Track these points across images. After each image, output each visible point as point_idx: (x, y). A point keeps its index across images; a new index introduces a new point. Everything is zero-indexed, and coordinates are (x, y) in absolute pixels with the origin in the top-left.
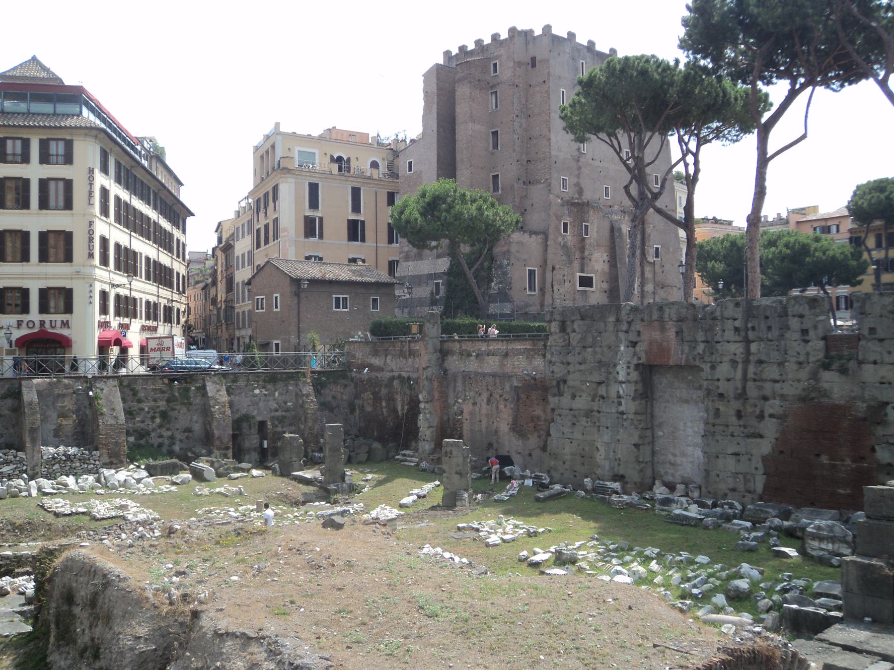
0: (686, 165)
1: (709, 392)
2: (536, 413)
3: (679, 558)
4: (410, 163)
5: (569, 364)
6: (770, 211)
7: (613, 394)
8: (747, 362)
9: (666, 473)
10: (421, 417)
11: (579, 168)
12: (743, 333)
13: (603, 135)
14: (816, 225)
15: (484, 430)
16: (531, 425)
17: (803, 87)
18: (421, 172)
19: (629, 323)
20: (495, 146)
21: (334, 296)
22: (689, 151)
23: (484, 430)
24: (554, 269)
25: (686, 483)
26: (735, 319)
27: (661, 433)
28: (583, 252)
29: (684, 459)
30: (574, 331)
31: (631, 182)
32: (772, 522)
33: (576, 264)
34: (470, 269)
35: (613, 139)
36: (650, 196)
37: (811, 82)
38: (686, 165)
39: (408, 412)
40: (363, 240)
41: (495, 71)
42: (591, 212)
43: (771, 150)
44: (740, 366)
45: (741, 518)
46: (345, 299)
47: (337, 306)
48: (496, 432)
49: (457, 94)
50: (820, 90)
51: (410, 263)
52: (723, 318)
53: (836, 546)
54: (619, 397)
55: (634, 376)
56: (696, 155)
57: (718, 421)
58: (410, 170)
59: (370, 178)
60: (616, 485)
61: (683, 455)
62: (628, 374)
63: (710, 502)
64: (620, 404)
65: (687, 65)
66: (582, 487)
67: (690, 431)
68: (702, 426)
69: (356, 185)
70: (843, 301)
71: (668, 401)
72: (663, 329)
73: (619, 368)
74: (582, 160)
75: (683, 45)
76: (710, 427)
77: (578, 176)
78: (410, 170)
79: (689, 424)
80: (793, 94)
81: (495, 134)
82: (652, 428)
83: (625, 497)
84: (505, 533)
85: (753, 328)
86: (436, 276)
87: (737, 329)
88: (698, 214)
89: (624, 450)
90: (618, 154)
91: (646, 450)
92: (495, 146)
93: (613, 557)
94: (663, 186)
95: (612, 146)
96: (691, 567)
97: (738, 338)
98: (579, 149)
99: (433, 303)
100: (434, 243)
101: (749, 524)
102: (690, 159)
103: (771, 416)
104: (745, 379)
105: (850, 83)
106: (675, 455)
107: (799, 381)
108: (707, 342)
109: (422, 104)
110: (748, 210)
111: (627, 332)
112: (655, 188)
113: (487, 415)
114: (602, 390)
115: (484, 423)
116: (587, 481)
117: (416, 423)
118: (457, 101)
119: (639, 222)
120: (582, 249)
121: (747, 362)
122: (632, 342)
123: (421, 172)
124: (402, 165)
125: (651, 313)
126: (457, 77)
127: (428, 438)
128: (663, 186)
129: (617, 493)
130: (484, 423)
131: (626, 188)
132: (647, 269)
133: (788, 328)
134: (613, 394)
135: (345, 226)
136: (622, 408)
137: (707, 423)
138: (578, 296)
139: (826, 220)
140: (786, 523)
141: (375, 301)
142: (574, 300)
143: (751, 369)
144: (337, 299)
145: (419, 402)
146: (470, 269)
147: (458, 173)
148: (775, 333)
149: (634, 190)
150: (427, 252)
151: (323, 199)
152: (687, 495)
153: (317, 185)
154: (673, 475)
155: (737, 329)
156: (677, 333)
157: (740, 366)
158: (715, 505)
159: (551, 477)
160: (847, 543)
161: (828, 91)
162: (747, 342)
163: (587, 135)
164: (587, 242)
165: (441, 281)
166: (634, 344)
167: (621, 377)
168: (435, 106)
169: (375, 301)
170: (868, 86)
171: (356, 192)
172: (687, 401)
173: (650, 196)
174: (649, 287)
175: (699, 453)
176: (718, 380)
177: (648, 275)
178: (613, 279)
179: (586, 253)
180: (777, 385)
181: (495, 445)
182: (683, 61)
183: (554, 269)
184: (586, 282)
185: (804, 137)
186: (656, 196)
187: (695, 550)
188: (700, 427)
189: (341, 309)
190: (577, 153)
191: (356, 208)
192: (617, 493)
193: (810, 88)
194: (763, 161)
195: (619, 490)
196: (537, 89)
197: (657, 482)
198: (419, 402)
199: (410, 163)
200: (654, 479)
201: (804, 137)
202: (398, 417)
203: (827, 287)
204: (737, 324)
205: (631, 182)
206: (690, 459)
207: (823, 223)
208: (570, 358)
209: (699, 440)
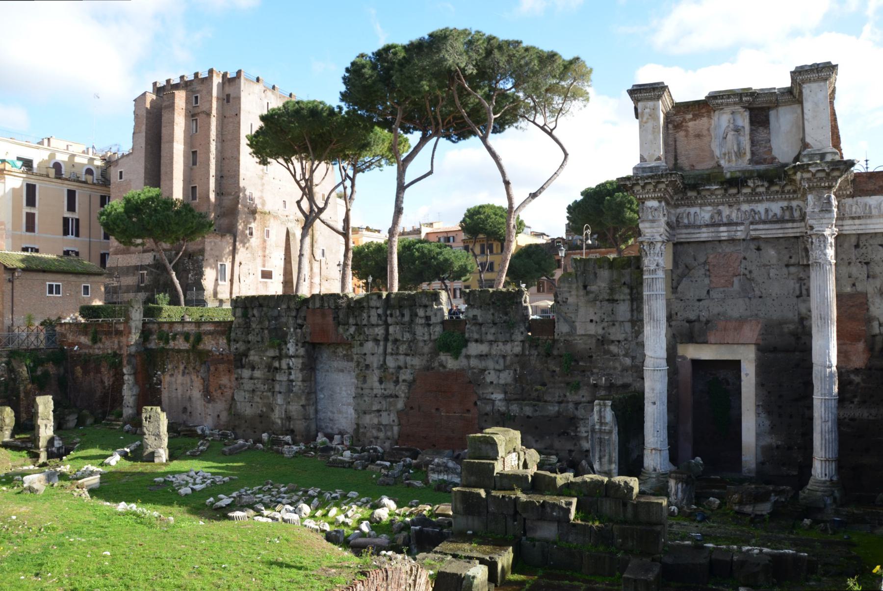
0: (345, 188)
1: (358, 364)
2: (222, 382)
3: (334, 495)
4: (121, 173)
5: (249, 342)
6: (406, 223)
7: (284, 366)
8: (386, 339)
9: (327, 427)
10: (125, 387)
11: (263, 185)
12: (383, 318)
13: (281, 160)
14: (440, 235)
15: (180, 396)
16: (219, 391)
17: (431, 136)
18: (130, 180)
19: (298, 310)
20: (194, 163)
21: (48, 283)
22: (347, 176)
23: (180, 396)
24: (240, 263)
25: (341, 433)
26: (377, 308)
27: (322, 396)
28: (264, 251)
29: (340, 416)
30: (254, 316)
31: (302, 198)
32: (404, 461)
33: (259, 261)
34: (170, 263)
35: (290, 165)
36: (316, 210)
37: (436, 133)
38: (345, 188)
39: (114, 382)
40: (77, 235)
41: (196, 102)
42: (272, 220)
43: (407, 180)
44: (382, 343)
45: (382, 460)
46: (58, 287)
47: (51, 292)
48: (190, 398)
49: (163, 118)
50: (443, 141)
51: (119, 256)
52: (369, 307)
53: (450, 477)
54: (289, 368)
55: (302, 351)
56: (353, 180)
57: (365, 386)
58: (121, 178)
59: (85, 182)
60: (288, 438)
61: (340, 412)
62: (297, 350)
63: (359, 449)
64: (290, 374)
65: (347, 113)
66: (260, 441)
67: (344, 394)
68: (353, 390)
69: (72, 188)
70: (458, 292)
71: (328, 371)
72: (324, 315)
73: (289, 345)
74: (265, 178)
75: (344, 97)
76: (360, 391)
77: (262, 191)
78: (121, 178)
79: (344, 388)
80: (424, 140)
81: (194, 153)
82: (315, 393)
83: (295, 448)
84: (195, 484)
85: (391, 315)
86: (142, 267)
87: (379, 315)
88: (353, 224)
89: (295, 408)
90: (294, 176)
91: (311, 410)
92: (194, 163)
93: (283, 498)
94: (326, 204)
95: (288, 169)
96: (345, 502)
97: (380, 322)
98: (263, 170)
99: (139, 289)
100: (139, 241)
101: (388, 464)
102: (348, 183)
103: (404, 381)
104: (385, 353)
105: (464, 139)
106: (333, 413)
107: (468, 257)
108: (356, 325)
109: (133, 124)
110: (390, 225)
111: (296, 317)
112: (321, 205)
113: (182, 384)
114: (276, 364)
115: (180, 391)
116: (265, 436)
117: (121, 392)
118: (163, 124)
119: (307, 226)
120: (264, 249)
121: (386, 339)
122: (299, 325)
123: (130, 180)
124: (114, 173)
125: (314, 303)
126: (164, 104)
127: (131, 404)
128: (326, 204)
129: (288, 444)
130: (180, 391)
131: (298, 203)
132: (316, 265)
133: (416, 315)
134: (284, 366)
135: (61, 222)
136: (292, 377)
137: (357, 388)
138: (260, 285)
139: (446, 232)
140: (414, 461)
141: (86, 288)
142: (257, 289)
143: (390, 346)
144: (51, 286)
145: (124, 374)
146: (170, 263)
147: (162, 183)
148: (407, 318)
149: (305, 204)
150: (132, 248)
151: (40, 199)
152: (342, 443)
153: (34, 186)
154: (332, 429)
155: (379, 315)
156: (334, 318)
157: (382, 343)
158: (363, 450)
159: (236, 434)
160: (457, 474)
161: (449, 142)
162: (387, 325)
163: (269, 160)
164: (268, 243)
165: (145, 272)
166: (301, 326)
167: (292, 351)
168: (144, 127)
169: (86, 288)
170: (474, 141)
171: (71, 195)
172: (342, 371)
173: (316, 210)
174: (317, 280)
175: (351, 411)
176: (365, 354)
177: (316, 270)
178: (287, 272)
179: (267, 252)
180: (408, 358)
181: (189, 409)
182: (345, 109)
183: (240, 263)
184: (267, 275)
185: (431, 173)
186: (321, 210)
187: (347, 488)
188: (352, 391)
189: (54, 295)
190: (261, 173)
191: (71, 207)
192: (288, 444)
193: (435, 139)
194: (401, 188)
195: (290, 442)
196: (231, 120)
197: (320, 434)
198: (124, 374)
199: (121, 173)
200: (317, 432)
201: (431, 173)
202: (104, 388)
203: (446, 281)
204: (380, 311)
205: (302, 198)
206: (345, 415)
207: (445, 235)
208: (250, 338)
209: (351, 400)
